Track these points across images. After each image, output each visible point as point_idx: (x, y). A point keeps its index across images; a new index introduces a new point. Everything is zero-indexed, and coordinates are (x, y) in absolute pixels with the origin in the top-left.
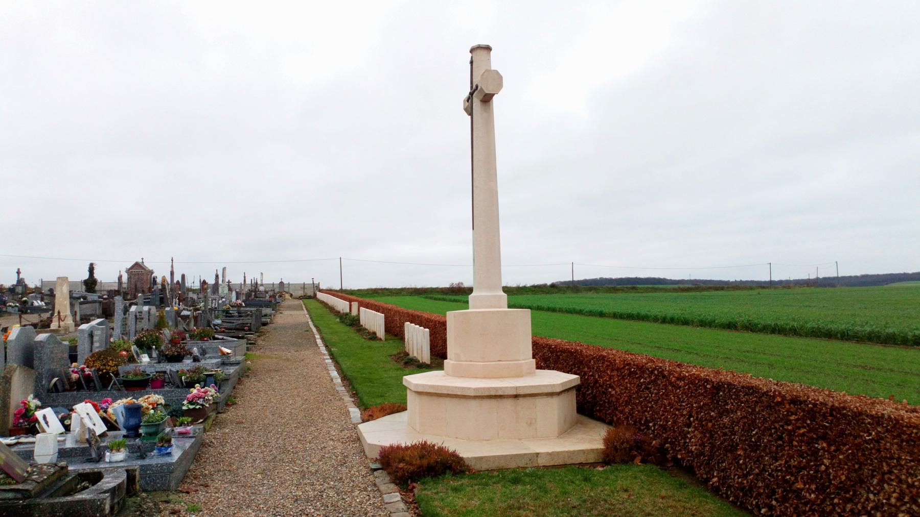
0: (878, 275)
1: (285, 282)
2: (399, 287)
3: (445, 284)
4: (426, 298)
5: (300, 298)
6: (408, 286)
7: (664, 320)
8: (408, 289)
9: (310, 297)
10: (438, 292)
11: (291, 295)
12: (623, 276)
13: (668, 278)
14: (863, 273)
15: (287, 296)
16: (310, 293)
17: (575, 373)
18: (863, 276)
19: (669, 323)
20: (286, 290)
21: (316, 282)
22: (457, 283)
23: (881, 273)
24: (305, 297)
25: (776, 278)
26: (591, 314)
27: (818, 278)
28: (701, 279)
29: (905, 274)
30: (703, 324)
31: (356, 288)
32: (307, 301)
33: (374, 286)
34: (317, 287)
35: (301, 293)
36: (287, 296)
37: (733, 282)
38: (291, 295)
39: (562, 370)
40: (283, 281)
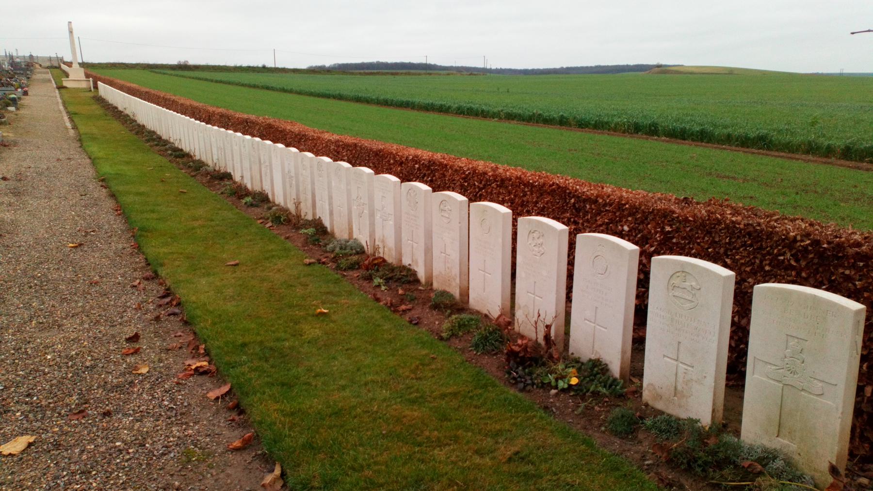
0: (608, 66)
1: (34, 55)
2: (134, 62)
3: (174, 61)
4: (151, 71)
5: (48, 68)
6: (513, 68)
7: (358, 100)
8: (142, 64)
9: (56, 67)
10: (168, 68)
11: (40, 65)
12: (398, 61)
13: (439, 64)
14: (597, 64)
15: (37, 66)
16: (56, 64)
17: (636, 243)
18: (596, 67)
19: (405, 107)
20: (36, 61)
21: (60, 56)
22: (184, 61)
23: (610, 64)
24: (51, 67)
25: (280, 65)
26: (217, 82)
27: (491, 69)
28: (820, 72)
29: (627, 66)
30: (284, 90)
31: (97, 62)
32: (51, 70)
33: (112, 61)
34: (61, 60)
35: (48, 64)
36: (37, 66)
37: (559, 69)
38: (40, 65)
39: (627, 238)
40: (32, 54)
